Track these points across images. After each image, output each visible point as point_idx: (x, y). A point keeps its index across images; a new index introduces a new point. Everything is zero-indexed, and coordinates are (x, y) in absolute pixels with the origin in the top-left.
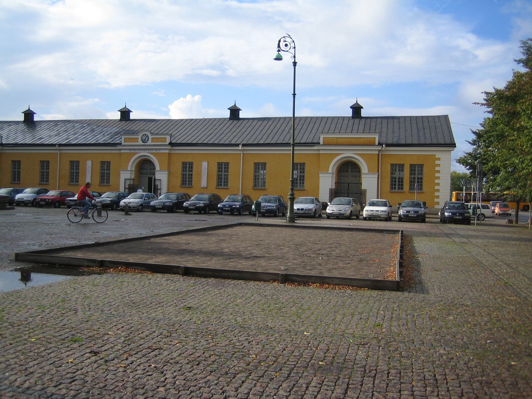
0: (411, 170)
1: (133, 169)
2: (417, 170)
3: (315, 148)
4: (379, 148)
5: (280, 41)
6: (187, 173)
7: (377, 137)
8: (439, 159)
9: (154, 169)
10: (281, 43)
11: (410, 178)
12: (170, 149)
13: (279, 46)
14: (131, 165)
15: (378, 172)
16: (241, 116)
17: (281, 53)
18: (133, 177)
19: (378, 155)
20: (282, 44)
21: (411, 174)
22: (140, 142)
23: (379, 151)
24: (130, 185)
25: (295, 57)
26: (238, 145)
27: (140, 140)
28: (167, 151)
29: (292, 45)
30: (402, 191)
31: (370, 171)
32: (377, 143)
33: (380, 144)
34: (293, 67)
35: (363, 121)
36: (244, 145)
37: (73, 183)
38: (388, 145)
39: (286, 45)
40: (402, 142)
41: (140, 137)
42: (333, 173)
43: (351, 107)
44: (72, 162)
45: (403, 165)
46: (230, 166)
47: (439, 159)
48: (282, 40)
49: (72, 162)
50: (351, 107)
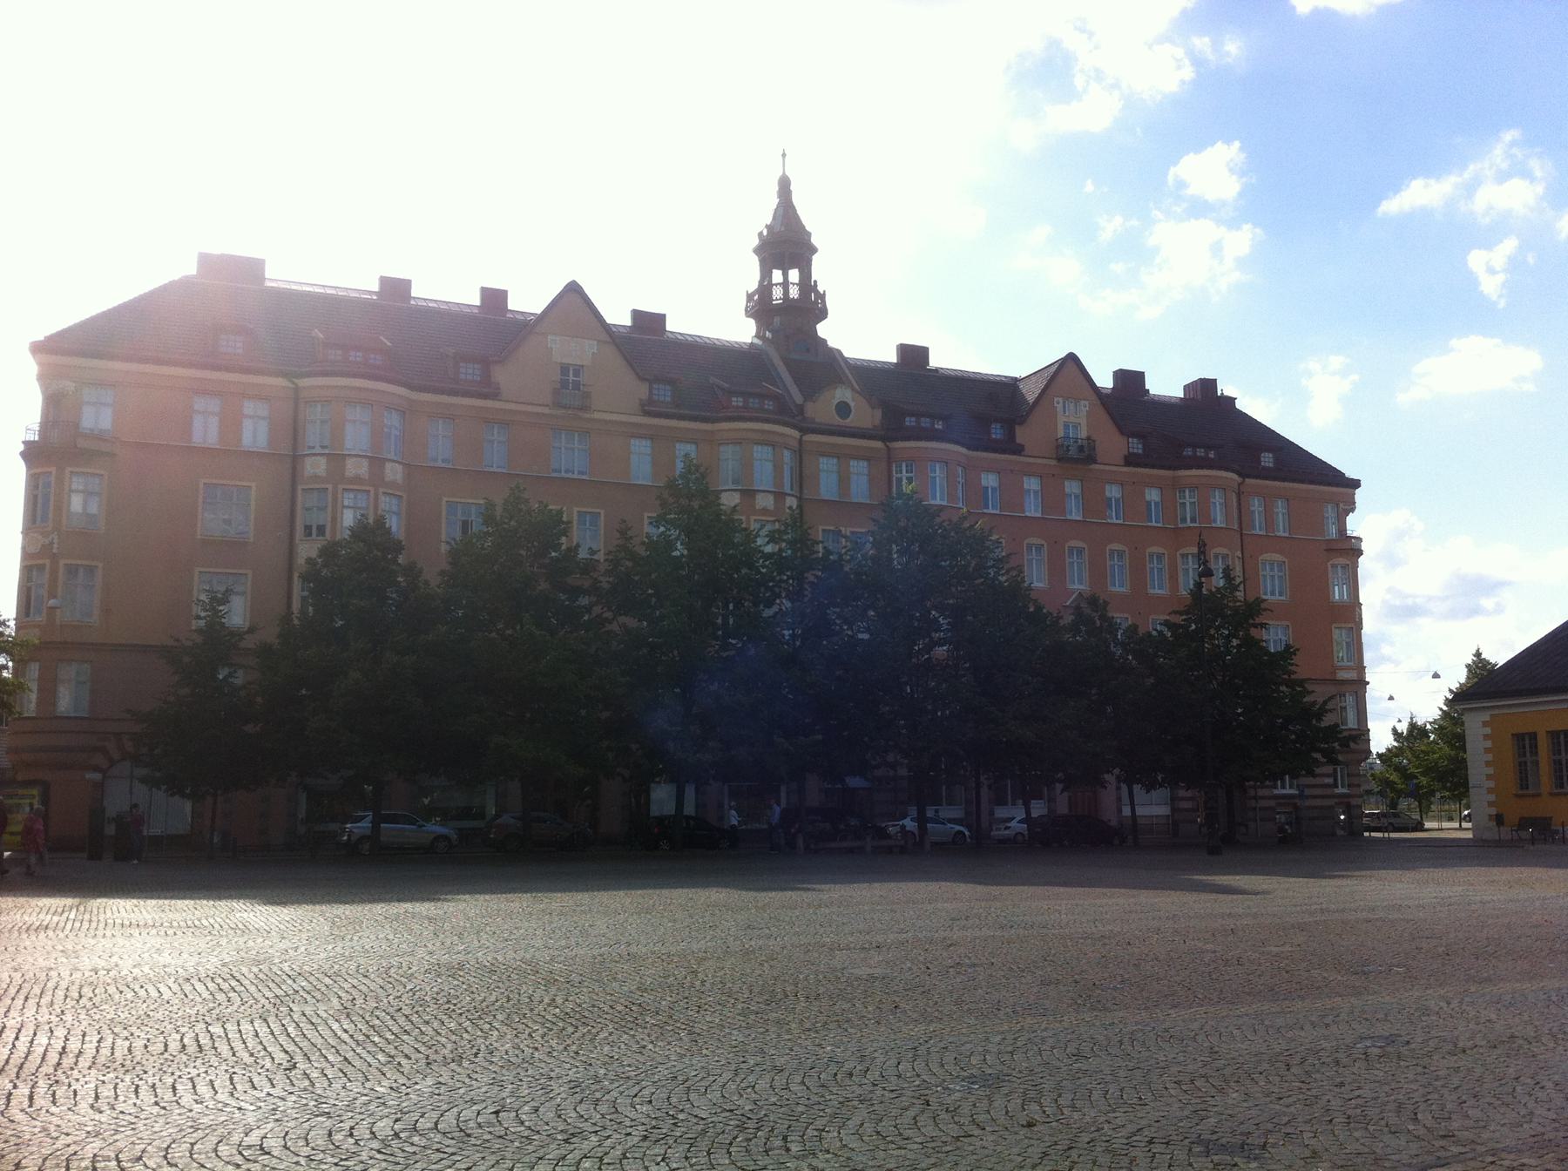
45: (1533, 736)
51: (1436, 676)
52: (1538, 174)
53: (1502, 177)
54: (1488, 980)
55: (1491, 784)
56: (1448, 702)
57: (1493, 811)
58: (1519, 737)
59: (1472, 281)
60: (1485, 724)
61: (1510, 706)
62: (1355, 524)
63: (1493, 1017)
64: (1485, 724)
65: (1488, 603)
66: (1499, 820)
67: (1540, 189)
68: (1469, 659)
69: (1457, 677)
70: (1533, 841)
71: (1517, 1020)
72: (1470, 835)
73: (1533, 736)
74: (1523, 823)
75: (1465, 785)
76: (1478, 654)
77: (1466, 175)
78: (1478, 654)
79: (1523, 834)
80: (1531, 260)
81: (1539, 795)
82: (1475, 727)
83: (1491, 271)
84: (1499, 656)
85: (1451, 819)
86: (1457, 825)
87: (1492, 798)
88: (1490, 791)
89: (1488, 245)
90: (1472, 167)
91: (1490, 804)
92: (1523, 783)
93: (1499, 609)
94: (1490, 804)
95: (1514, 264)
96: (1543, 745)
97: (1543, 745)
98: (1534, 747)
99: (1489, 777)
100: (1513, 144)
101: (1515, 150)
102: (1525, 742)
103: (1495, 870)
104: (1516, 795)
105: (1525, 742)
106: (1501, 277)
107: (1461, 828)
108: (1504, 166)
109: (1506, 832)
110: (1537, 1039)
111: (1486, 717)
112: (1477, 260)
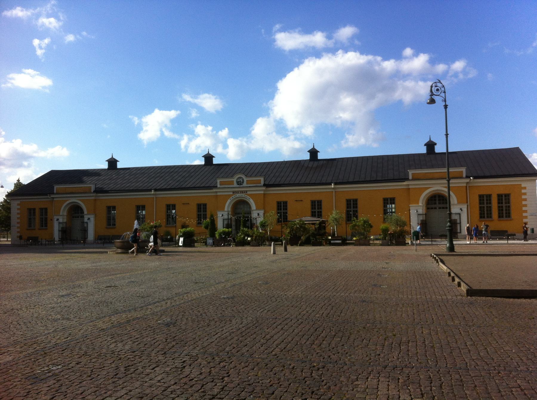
0: (499, 200)
1: (230, 210)
2: (504, 200)
3: (214, 190)
4: (467, 180)
5: (432, 87)
6: (202, 213)
7: (262, 179)
8: (525, 188)
9: (250, 207)
10: (433, 89)
11: (499, 207)
12: (96, 196)
13: (431, 91)
14: (228, 206)
15: (467, 202)
16: (319, 158)
17: (435, 97)
18: (65, 221)
19: (466, 187)
20: (434, 89)
21: (499, 203)
22: (235, 185)
23: (467, 183)
24: (62, 228)
25: (445, 101)
26: (150, 190)
27: (235, 183)
28: (262, 192)
29: (443, 89)
30: (490, 219)
31: (459, 202)
32: (464, 175)
33: (265, 185)
34: (444, 109)
35: (213, 167)
36: (156, 190)
37: (111, 227)
38: (475, 178)
39: (438, 90)
40: (351, 180)
41: (235, 180)
42: (423, 206)
43: (425, 145)
44: (481, 197)
45: (34, 209)
46: (208, 206)
47: (525, 188)
48: (434, 85)
49: (481, 197)
50: (425, 145)
51: (2, 187)
52: (62, 18)
53: (48, 16)
54: (8, 291)
55: (19, 225)
56: (7, 196)
57: (19, 235)
58: (30, 210)
59: (34, 49)
60: (18, 205)
61: (143, 195)
62: (157, 111)
63: (7, 303)
64: (18, 205)
65: (26, 163)
66: (21, 237)
67: (61, 24)
68: (16, 182)
69: (10, 188)
70: (31, 245)
71: (15, 304)
72: (10, 243)
73: (34, 209)
74: (28, 239)
75: (10, 225)
76: (18, 181)
77: (36, 11)
78: (18, 181)
79: (28, 243)
80: (55, 47)
81: (35, 229)
82: (15, 205)
83: (40, 48)
84: (25, 181)
85: (4, 237)
86: (6, 239)
87: (19, 230)
88: (18, 227)
89: (41, 38)
90: (38, 9)
91: (18, 232)
92: (30, 225)
93: (29, 166)
94: (18, 232)
95: (49, 47)
96: (352, 201)
97: (37, 211)
98: (34, 213)
99: (18, 223)
100: (54, 5)
101: (54, 8)
102: (31, 211)
103: (16, 255)
104: (106, 228)
105: (31, 211)
106: (43, 51)
107: (7, 241)
108: (50, 12)
109: (22, 242)
110: (21, 309)
111: (18, 202)
112: (36, 42)
